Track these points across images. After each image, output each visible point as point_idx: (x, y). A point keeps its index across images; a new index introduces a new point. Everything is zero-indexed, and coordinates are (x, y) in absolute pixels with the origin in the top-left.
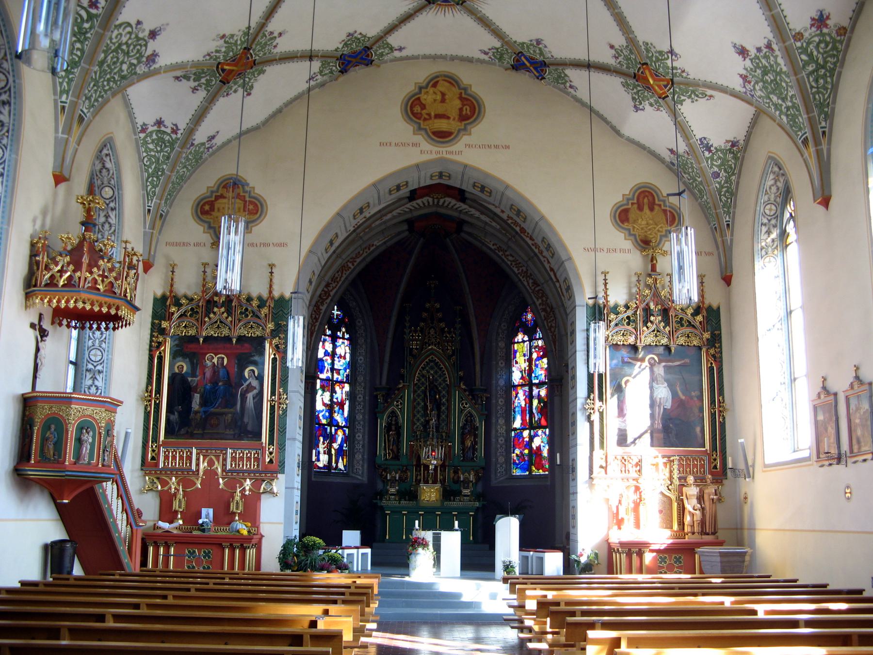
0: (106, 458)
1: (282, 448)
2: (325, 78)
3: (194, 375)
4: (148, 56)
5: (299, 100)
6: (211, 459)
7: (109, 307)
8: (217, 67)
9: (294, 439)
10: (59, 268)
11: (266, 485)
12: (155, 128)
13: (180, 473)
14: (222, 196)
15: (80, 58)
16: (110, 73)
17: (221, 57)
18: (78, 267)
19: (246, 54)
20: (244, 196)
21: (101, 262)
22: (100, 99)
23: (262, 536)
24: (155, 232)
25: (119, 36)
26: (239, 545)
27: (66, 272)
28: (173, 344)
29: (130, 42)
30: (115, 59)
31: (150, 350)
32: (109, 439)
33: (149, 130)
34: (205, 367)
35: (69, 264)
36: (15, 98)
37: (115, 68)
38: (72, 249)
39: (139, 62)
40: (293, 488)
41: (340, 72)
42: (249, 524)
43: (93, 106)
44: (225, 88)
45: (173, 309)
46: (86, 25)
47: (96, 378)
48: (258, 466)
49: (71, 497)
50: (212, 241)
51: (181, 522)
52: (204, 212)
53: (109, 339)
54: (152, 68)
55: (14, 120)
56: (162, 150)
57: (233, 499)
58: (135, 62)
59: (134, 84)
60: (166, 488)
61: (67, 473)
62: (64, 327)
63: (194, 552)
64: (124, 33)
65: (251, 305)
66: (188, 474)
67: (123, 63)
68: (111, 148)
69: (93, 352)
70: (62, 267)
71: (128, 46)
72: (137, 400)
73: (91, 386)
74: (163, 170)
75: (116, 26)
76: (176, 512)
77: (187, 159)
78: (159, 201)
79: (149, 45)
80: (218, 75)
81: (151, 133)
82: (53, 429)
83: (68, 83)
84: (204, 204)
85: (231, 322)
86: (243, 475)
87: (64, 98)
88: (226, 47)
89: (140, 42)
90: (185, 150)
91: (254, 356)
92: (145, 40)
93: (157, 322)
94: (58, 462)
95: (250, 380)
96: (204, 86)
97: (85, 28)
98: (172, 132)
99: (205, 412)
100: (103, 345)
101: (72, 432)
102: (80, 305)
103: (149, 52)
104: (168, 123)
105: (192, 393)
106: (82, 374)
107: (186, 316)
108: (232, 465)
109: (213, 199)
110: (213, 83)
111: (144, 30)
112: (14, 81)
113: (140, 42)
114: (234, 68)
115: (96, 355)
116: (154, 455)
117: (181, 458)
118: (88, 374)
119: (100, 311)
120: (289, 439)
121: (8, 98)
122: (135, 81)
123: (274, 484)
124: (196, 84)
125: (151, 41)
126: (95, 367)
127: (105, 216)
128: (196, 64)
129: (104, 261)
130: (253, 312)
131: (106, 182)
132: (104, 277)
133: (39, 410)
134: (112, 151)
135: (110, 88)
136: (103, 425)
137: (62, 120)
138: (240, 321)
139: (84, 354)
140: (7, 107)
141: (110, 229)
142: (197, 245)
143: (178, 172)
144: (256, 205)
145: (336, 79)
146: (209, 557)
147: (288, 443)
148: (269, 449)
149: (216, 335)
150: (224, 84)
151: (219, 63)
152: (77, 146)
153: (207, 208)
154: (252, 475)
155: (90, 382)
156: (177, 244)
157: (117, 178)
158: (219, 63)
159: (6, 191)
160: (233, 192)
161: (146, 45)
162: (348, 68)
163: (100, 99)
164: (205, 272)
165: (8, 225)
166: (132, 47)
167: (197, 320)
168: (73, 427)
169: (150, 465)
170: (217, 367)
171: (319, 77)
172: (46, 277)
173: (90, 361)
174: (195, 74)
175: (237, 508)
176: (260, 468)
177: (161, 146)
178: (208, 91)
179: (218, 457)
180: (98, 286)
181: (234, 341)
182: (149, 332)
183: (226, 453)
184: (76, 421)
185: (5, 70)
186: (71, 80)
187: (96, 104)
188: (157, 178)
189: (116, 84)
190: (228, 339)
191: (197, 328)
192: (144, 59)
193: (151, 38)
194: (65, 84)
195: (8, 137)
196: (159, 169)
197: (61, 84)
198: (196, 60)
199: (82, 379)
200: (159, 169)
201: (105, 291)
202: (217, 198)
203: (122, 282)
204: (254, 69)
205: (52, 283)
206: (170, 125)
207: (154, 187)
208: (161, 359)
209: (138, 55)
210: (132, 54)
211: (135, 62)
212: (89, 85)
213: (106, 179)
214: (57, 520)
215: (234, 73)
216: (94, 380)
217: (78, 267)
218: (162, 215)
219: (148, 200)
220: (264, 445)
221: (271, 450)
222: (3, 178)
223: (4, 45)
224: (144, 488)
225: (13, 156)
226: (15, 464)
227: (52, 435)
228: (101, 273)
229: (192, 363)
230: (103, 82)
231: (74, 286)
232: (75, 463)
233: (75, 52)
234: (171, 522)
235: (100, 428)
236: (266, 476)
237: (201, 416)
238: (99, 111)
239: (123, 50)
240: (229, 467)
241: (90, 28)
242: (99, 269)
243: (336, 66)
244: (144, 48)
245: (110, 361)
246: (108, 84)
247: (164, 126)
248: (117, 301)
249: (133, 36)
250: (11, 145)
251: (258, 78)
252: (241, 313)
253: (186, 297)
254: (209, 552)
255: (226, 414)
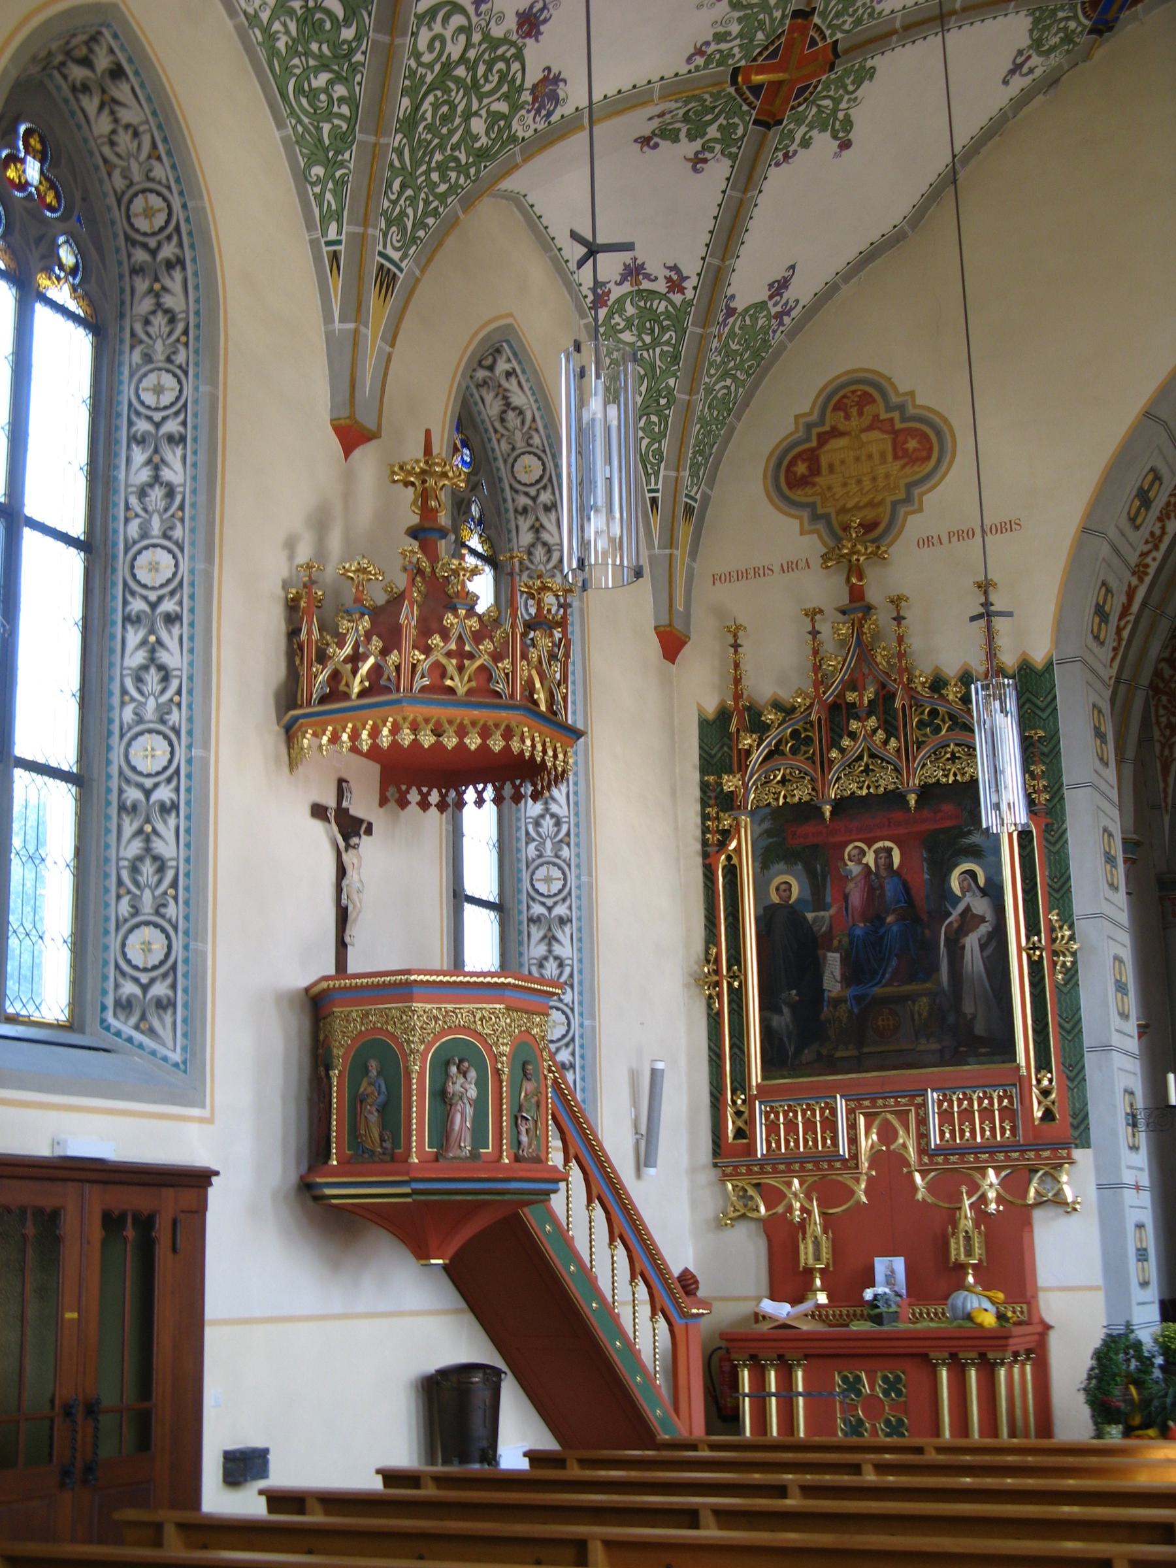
0: (524, 1139)
1: (1075, 1074)
2: (1055, 59)
3: (819, 904)
4: (535, 86)
5: (997, 139)
6: (887, 1122)
7: (485, 733)
8: (734, 81)
9: (1107, 1048)
10: (348, 650)
11: (1041, 1181)
12: (627, 287)
13: (810, 1166)
14: (835, 433)
15: (351, 121)
16: (441, 147)
17: (736, 50)
18: (391, 642)
19: (804, 31)
20: (891, 420)
21: (449, 619)
22: (430, 221)
23: (1048, 1327)
24: (677, 553)
25: (437, 45)
26: (973, 1355)
27: (365, 658)
28: (759, 830)
29: (472, 54)
30: (445, 109)
31: (705, 855)
32: (528, 1086)
33: (613, 297)
34: (845, 879)
35: (368, 636)
36: (192, 246)
37: (451, 132)
38: (388, 602)
39: (515, 107)
40: (1120, 1186)
41: (1091, 32)
42: (1001, 1296)
43: (414, 240)
44: (774, 135)
45: (747, 741)
46: (348, 34)
47: (554, 938)
48: (1014, 1130)
49: (451, 1251)
50: (824, 550)
51: (822, 1298)
52: (797, 483)
53: (577, 835)
54: (555, 118)
55: (197, 301)
56: (656, 342)
57: (955, 1225)
58: (503, 107)
59: (517, 167)
60: (780, 1209)
61: (416, 1186)
62: (413, 808)
63: (858, 1379)
64: (448, 35)
65: (943, 697)
66: (831, 1167)
67: (468, 115)
68: (515, 354)
69: (541, 873)
70: (356, 646)
71: (472, 67)
72: (687, 986)
73: (546, 958)
74: (670, 391)
75: (420, 18)
76: (961, 1268)
77: (729, 354)
78: (673, 474)
79: (527, 53)
80: (745, 108)
81: (621, 301)
82: (374, 1073)
83: (334, 192)
84: (793, 463)
85: (898, 751)
86: (977, 1160)
87: (332, 234)
88: (740, 20)
89: (500, 52)
90: (714, 330)
91: (970, 833)
92: (513, 44)
93: (712, 779)
94: (393, 1158)
95: (968, 899)
96: (718, 147)
97: (345, 42)
98: (671, 289)
99: (858, 999)
100: (565, 852)
101: (421, 1074)
102: (406, 737)
103: (533, 76)
104: (654, 267)
105: (820, 952)
106: (520, 932)
107: (783, 754)
108: (942, 1133)
109: (814, 444)
110: (740, 132)
111: (501, 18)
112: (184, 206)
113: (500, 52)
114: (780, 76)
115: (548, 881)
116: (740, 1123)
117: (809, 1125)
118: (534, 929)
119: (461, 745)
120: (1093, 1049)
121: (177, 251)
122: (519, 159)
123: (1064, 1178)
124: (697, 145)
125: (530, 42)
126: (550, 909)
127: (532, 527)
128: (672, 88)
129: (456, 616)
130: (952, 717)
131: (520, 444)
132: (462, 656)
133: (338, 1025)
134: (520, 363)
135: (453, 189)
136: (506, 1049)
137: (336, 286)
138: (920, 745)
139: (520, 880)
140: (177, 274)
141: (549, 560)
142: (789, 567)
143: (709, 390)
144: (924, 437)
145: (1087, 57)
146: (899, 1393)
147: (1090, 1060)
148: (1039, 1081)
149: (865, 792)
150: (768, 126)
151: (736, 71)
152: (388, 349)
153: (801, 468)
154: (1001, 1156)
155: (540, 950)
156: (741, 575)
157: (545, 427)
158: (736, 71)
159: (194, 478)
160: (860, 414)
161: (519, 57)
162: (1111, 15)
163: (430, 221)
164: (814, 633)
165: (210, 559)
166: (481, 69)
167: (811, 759)
168: (424, 1061)
169: (734, 1152)
170: (877, 874)
171: (1036, 60)
172: (321, 678)
173: (535, 895)
174: (686, 118)
175: (969, 1253)
176: (1020, 1138)
177: (653, 331)
178: (733, 157)
179: (903, 1116)
180: (449, 682)
181: (912, 799)
182: (698, 807)
183: (924, 1104)
184: (429, 1046)
185: (160, 183)
186: (341, 183)
187: (421, 233)
188: (659, 414)
189: (468, 176)
190: (895, 798)
191: (813, 780)
192: (526, 96)
193: (528, 35)
194: (329, 196)
195: (186, 344)
196: (659, 391)
197: (320, 198)
198: (668, 73)
199: (521, 943)
200: (659, 391)
201: (470, 692)
202: (823, 439)
203: (513, 663)
204: (839, 70)
205: (335, 692)
206: (662, 273)
207: (656, 438)
208: (732, 872)
209: (505, 88)
210: (488, 87)
211: (503, 107)
212: (389, 186)
213: (518, 435)
214: (457, 1311)
215: (785, 89)
216: (550, 944)
217: (391, 642)
218: (689, 510)
219: (647, 475)
220: (1024, 1072)
221: (1045, 1082)
222: (185, 448)
223: (147, 122)
224: (725, 1214)
225: (204, 388)
226: (304, 1169)
227: (374, 1089)
228: (453, 646)
229: (811, 873)
230: (427, 173)
231: (387, 690)
232: (436, 1158)
233: (336, 109)
234: (795, 1301)
235: (495, 1058)
236: (1038, 1157)
237: (851, 1012)
238: (435, 251)
239: (458, 81)
240: (935, 1140)
241: (358, 37)
242: (445, 637)
243: (1075, 17)
244: (516, 66)
245: (588, 890)
246: (444, 178)
247: (648, 277)
248: (504, 714)
249: (476, 38)
250: (197, 364)
251: (859, 93)
252: (922, 724)
253: (777, 705)
254: (898, 1378)
255: (912, 997)
